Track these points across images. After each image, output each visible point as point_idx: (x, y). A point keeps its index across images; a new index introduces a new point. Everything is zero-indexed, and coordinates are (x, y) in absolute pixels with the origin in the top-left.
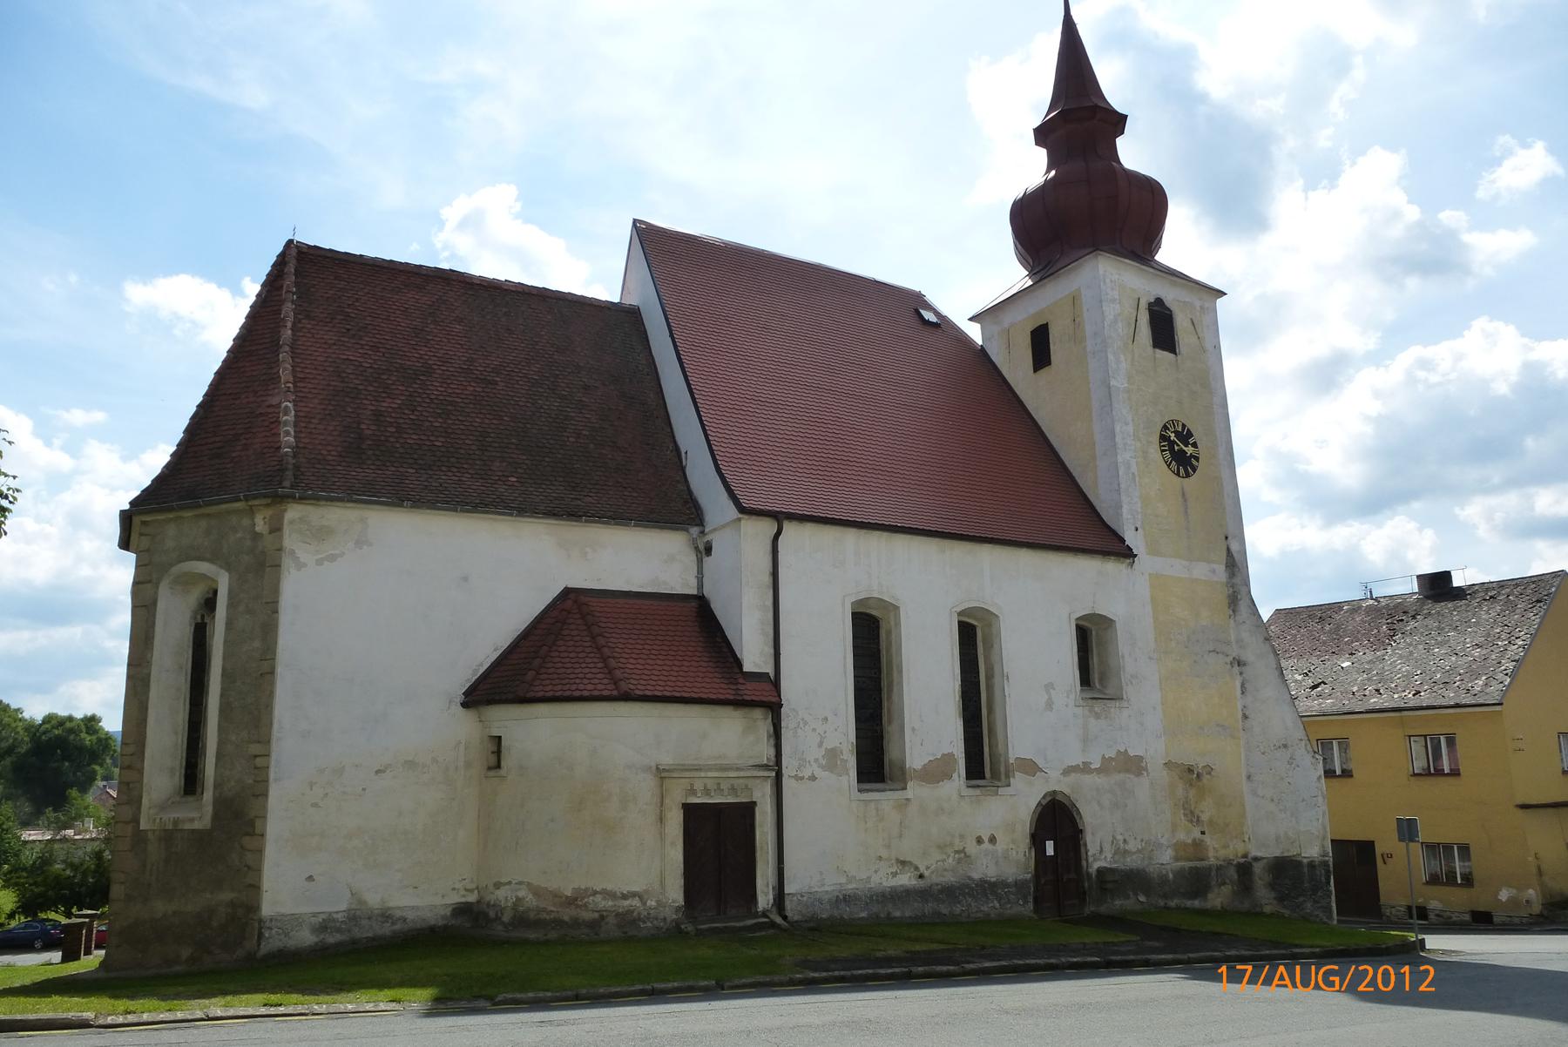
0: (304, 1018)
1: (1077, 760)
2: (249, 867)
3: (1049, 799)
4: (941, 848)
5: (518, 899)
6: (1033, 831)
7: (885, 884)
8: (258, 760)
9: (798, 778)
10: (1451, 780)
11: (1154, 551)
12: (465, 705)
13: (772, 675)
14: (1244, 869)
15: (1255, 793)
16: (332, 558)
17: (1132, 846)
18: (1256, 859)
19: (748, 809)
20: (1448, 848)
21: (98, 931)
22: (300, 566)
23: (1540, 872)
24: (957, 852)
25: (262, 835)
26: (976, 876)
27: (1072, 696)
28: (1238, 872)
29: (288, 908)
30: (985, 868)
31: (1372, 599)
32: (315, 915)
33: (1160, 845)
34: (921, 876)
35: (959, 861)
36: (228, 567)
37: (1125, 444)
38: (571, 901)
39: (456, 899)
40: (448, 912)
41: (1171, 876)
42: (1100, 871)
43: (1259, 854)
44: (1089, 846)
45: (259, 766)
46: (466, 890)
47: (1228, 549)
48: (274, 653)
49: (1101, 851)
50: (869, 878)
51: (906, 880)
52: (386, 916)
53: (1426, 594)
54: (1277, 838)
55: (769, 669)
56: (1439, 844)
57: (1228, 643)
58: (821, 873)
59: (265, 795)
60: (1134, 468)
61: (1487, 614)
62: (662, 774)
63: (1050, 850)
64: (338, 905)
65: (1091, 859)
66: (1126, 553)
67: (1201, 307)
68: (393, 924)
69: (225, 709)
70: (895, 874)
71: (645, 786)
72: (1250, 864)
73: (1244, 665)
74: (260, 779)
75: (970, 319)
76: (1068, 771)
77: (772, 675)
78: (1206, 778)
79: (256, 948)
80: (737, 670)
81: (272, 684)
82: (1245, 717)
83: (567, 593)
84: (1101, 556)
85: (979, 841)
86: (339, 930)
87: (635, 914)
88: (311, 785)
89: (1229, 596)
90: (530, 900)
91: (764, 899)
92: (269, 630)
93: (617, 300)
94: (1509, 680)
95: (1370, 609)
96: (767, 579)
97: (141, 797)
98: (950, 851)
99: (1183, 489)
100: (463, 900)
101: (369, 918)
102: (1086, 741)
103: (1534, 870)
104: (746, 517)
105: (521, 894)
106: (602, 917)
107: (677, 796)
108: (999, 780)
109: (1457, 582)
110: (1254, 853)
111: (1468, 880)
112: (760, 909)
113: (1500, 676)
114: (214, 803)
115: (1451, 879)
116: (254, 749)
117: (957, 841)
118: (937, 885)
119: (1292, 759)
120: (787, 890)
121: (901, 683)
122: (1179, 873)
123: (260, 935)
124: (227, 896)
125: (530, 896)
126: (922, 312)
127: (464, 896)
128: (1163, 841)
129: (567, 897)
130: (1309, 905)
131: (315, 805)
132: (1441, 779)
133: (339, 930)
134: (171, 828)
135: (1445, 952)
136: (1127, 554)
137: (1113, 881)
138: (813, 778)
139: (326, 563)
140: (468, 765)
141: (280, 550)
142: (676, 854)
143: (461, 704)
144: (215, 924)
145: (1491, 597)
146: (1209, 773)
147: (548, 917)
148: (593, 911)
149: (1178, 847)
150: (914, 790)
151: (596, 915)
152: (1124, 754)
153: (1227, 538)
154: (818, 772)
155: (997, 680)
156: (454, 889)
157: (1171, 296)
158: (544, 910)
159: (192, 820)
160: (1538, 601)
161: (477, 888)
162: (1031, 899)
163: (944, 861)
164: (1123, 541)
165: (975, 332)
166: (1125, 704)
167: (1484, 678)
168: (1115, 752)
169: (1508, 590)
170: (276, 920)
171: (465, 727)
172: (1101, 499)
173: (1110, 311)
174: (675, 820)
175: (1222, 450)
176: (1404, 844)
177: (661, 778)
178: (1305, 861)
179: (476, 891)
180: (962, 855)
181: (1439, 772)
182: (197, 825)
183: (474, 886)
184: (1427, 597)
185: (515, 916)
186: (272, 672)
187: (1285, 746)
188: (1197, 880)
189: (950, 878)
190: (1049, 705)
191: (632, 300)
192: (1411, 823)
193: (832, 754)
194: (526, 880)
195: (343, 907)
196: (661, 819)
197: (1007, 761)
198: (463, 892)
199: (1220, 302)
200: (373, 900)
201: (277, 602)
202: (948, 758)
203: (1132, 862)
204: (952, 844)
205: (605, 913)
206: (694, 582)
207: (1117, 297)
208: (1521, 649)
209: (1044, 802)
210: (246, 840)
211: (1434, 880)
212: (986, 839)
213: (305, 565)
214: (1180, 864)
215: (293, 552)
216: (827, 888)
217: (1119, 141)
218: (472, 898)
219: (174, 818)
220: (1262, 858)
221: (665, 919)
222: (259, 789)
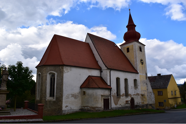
5: (88, 108)
11: (140, 73)
16: (68, 72)
20: (161, 103)
22: (65, 72)
36: (56, 72)
55: (109, 85)
59: (62, 97)
62: (102, 96)
66: (138, 73)
69: (57, 88)
76: (133, 95)
83: (89, 76)
91: (110, 108)
92: (62, 79)
102: (135, 92)
119: (151, 94)
120: (112, 107)
136: (138, 73)
137: (137, 106)
141: (63, 71)
142: (103, 104)
149: (142, 102)
165: (120, 47)
172: (135, 66)
173: (136, 47)
174: (103, 100)
186: (63, 84)
188: (143, 106)
189: (124, 106)
190: (132, 88)
192: (165, 100)
196: (102, 100)
206: (100, 75)
217: (135, 28)
218: (81, 108)
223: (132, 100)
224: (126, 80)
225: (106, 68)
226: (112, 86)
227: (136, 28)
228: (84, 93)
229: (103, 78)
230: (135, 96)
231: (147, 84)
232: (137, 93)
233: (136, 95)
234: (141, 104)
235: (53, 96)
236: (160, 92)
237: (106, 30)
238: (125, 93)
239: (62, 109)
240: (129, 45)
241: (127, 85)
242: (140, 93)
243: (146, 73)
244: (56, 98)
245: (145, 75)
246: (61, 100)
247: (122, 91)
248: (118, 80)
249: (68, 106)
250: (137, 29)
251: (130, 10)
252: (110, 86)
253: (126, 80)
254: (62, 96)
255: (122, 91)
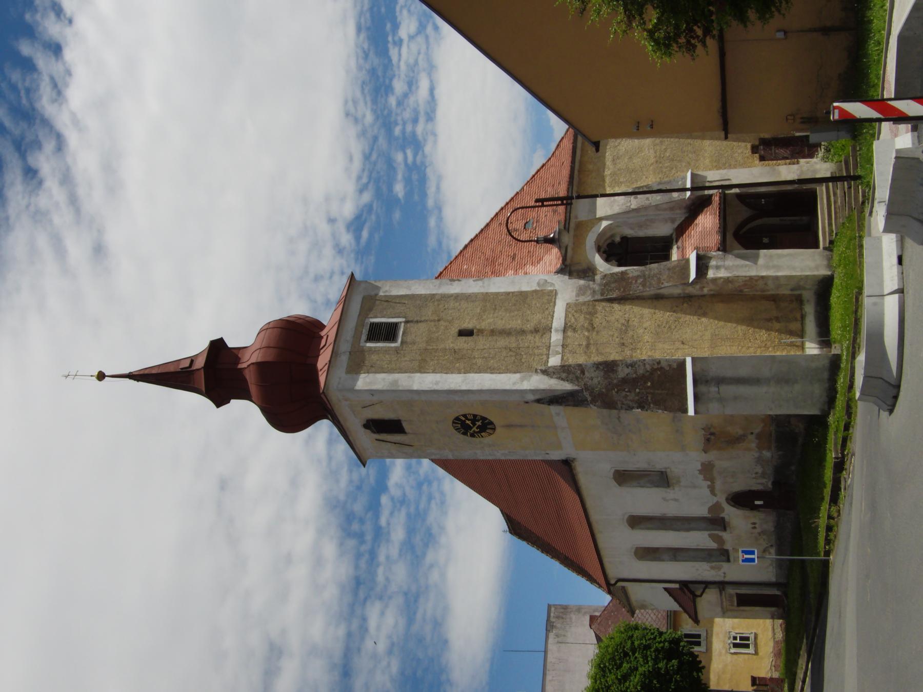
3: (731, 502)
6: (551, 556)
9: (725, 577)
17: (759, 470)
21: (824, 556)
26: (773, 529)
30: (770, 526)
34: (772, 546)
76: (713, 492)
78: (712, 430)
84: (576, 477)
85: (754, 528)
99: (131, 376)
135: (847, 549)
142: (757, 608)
149: (760, 448)
166: (668, 470)
190: (676, 500)
209: (732, 504)
223: (742, 500)
230: (718, 484)
232: (701, 472)
233: (712, 480)
234: (767, 454)
243: (539, 401)
247: (700, 539)
251: (101, 376)
255: (700, 539)
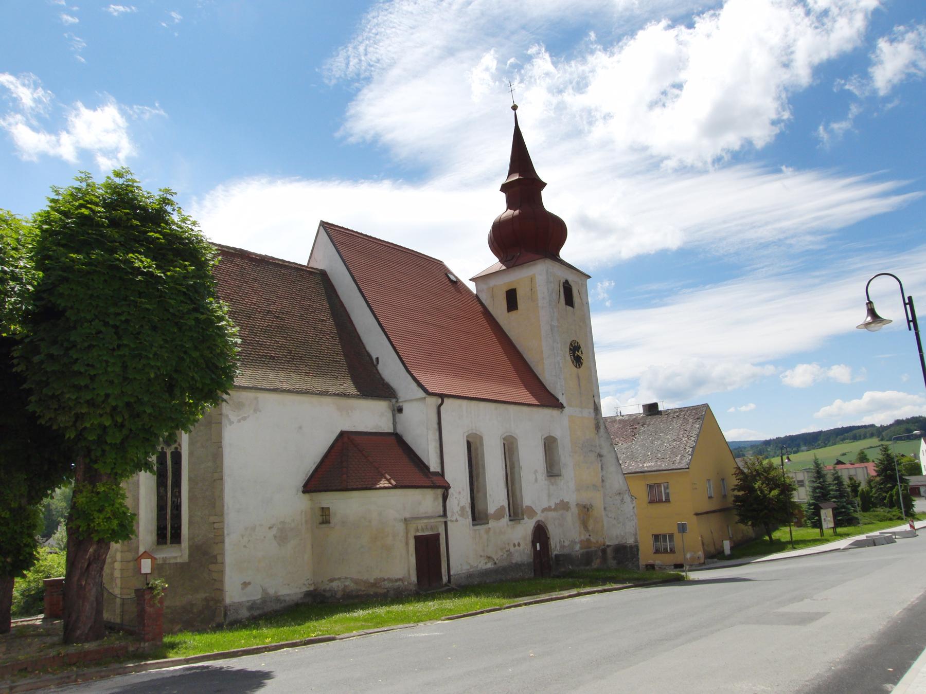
0: (348, 639)
1: (546, 505)
2: (215, 580)
3: (537, 524)
4: (502, 549)
5: (345, 586)
7: (483, 568)
8: (216, 526)
10: (667, 505)
12: (304, 492)
13: (440, 472)
14: (604, 551)
15: (607, 515)
16: (244, 419)
18: (608, 546)
19: (437, 536)
20: (664, 536)
22: (231, 423)
23: (703, 544)
24: (507, 551)
25: (223, 563)
26: (514, 562)
27: (544, 475)
28: (602, 553)
29: (237, 599)
30: (517, 558)
31: (621, 416)
32: (248, 602)
33: (575, 542)
34: (495, 563)
35: (508, 555)
37: (558, 353)
38: (374, 585)
39: (305, 589)
40: (302, 596)
41: (580, 556)
42: (556, 556)
43: (609, 544)
44: (552, 545)
45: (217, 528)
46: (309, 585)
47: (594, 402)
48: (222, 468)
49: (556, 547)
50: (478, 565)
51: (490, 565)
52: (277, 599)
53: (647, 414)
54: (617, 537)
55: (439, 470)
56: (660, 534)
57: (596, 446)
58: (461, 565)
59: (223, 542)
60: (561, 365)
61: (676, 424)
63: (538, 548)
64: (257, 596)
65: (552, 551)
66: (561, 406)
67: (582, 284)
68: (281, 603)
69: (191, 499)
70: (486, 563)
71: (401, 527)
72: (606, 548)
73: (602, 456)
74: (217, 535)
75: (470, 280)
76: (544, 510)
77: (440, 472)
79: (223, 621)
80: (427, 471)
81: (222, 485)
82: (603, 481)
83: (342, 434)
85: (514, 545)
86: (258, 608)
87: (401, 588)
88: (243, 536)
89: (595, 424)
90: (352, 586)
91: (445, 579)
92: (217, 456)
93: (304, 262)
94: (690, 457)
95: (620, 421)
96: (436, 426)
97: (138, 548)
98: (504, 551)
100: (308, 589)
101: (271, 602)
102: (549, 496)
103: (700, 543)
104: (429, 396)
105: (347, 584)
106: (388, 591)
107: (412, 534)
108: (519, 516)
109: (660, 408)
110: (608, 543)
111: (672, 551)
112: (444, 583)
113: (686, 455)
114: (189, 548)
115: (665, 551)
116: (213, 519)
117: (507, 546)
118: (501, 567)
119: (622, 500)
120: (451, 573)
121: (484, 473)
122: (582, 555)
123: (225, 614)
124: (201, 595)
125: (352, 584)
126: (449, 275)
127: (308, 588)
128: (577, 540)
129: (371, 583)
130: (630, 565)
131: (245, 546)
132: (662, 504)
133: (258, 608)
134: (161, 562)
136: (561, 406)
138: (457, 521)
139: (242, 421)
140: (306, 522)
141: (221, 414)
142: (413, 560)
143: (302, 492)
144: (195, 610)
145: (677, 416)
146: (591, 508)
147: (363, 593)
148: (384, 589)
149: (581, 542)
150: (492, 524)
151: (386, 590)
152: (562, 501)
153: (594, 396)
154: (459, 518)
155: (516, 469)
156: (304, 584)
157: (571, 278)
158: (360, 590)
159: (175, 558)
160: (698, 419)
161: (314, 583)
162: (533, 571)
163: (503, 555)
164: (558, 400)
165: (472, 287)
166: (562, 478)
167: (679, 456)
168: (559, 500)
169: (684, 413)
170: (232, 605)
171: (303, 503)
174: (412, 543)
175: (591, 354)
176: (681, 534)
177: (475, 530)
178: (628, 545)
179: (313, 585)
180: (509, 552)
181: (660, 501)
182: (179, 560)
183: (312, 582)
184: (648, 415)
185: (344, 594)
186: (221, 479)
187: (620, 493)
189: (505, 563)
190: (536, 480)
191: (320, 265)
193: (463, 508)
194: (349, 576)
195: (259, 597)
196: (407, 544)
197: (522, 507)
198: (308, 586)
199: (588, 280)
200: (271, 591)
201: (221, 442)
202: (502, 507)
203: (566, 551)
204: (505, 548)
205: (389, 589)
206: (392, 426)
207: (552, 280)
208: (693, 442)
210: (212, 567)
211: (657, 551)
212: (517, 544)
213: (233, 423)
214: (583, 550)
215: (227, 416)
216: (464, 572)
217: (543, 192)
218: (312, 588)
219: (163, 558)
220: (610, 546)
221: (411, 590)
222: (219, 538)
223: (540, 533)
224: (509, 448)
225: (421, 394)
226: (448, 477)
227: (545, 194)
228: (325, 517)
229: (409, 439)
231: (600, 456)
234: (577, 547)
235: (176, 538)
236: (659, 485)
237: (864, 451)
238: (505, 504)
239: (223, 600)
240: (520, 277)
241: (512, 468)
242: (572, 498)
244: (190, 547)
245: (593, 414)
246: (215, 557)
248: (473, 450)
249: (249, 583)
250: (551, 202)
251: (515, 108)
252: (442, 474)
253: (509, 448)
254: (223, 536)
